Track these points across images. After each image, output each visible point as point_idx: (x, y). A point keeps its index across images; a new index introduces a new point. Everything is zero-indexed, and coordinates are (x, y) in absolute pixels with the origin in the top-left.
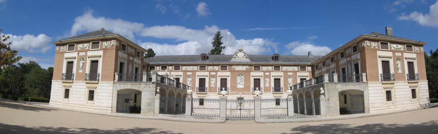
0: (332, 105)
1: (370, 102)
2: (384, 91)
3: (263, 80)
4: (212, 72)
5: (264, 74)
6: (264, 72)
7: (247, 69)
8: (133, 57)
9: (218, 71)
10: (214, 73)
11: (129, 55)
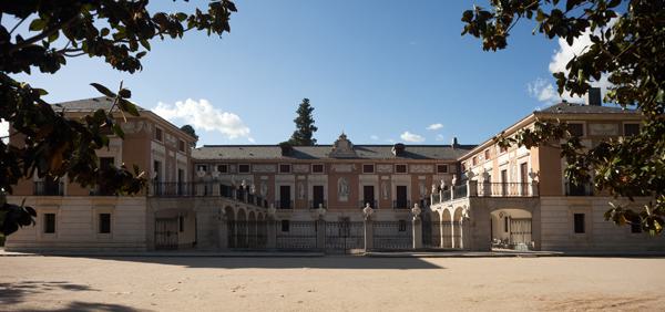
6: (297, 175)
8: (175, 150)
9: (309, 173)
10: (387, 178)
11: (168, 148)
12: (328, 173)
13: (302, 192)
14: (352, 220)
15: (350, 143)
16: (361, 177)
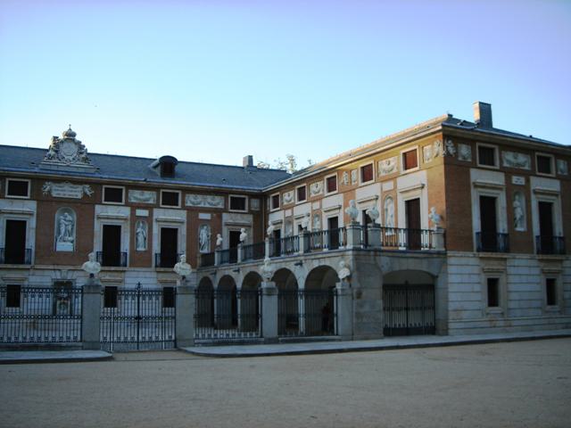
0: (366, 308)
1: (451, 306)
2: (484, 279)
3: (129, 228)
6: (134, 207)
7: (85, 194)
10: (145, 213)
12: (37, 196)
15: (80, 147)
16: (98, 209)
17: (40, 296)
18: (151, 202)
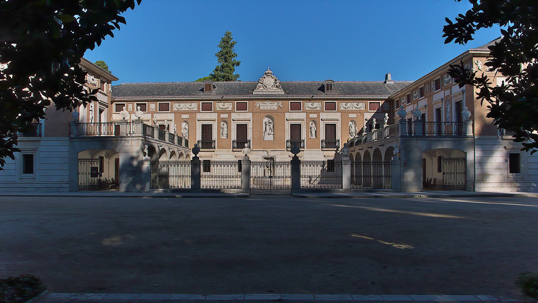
4: (311, 113)
5: (307, 116)
6: (219, 113)
13: (225, 132)
14: (277, 160)
17: (314, 166)
18: (318, 109)
